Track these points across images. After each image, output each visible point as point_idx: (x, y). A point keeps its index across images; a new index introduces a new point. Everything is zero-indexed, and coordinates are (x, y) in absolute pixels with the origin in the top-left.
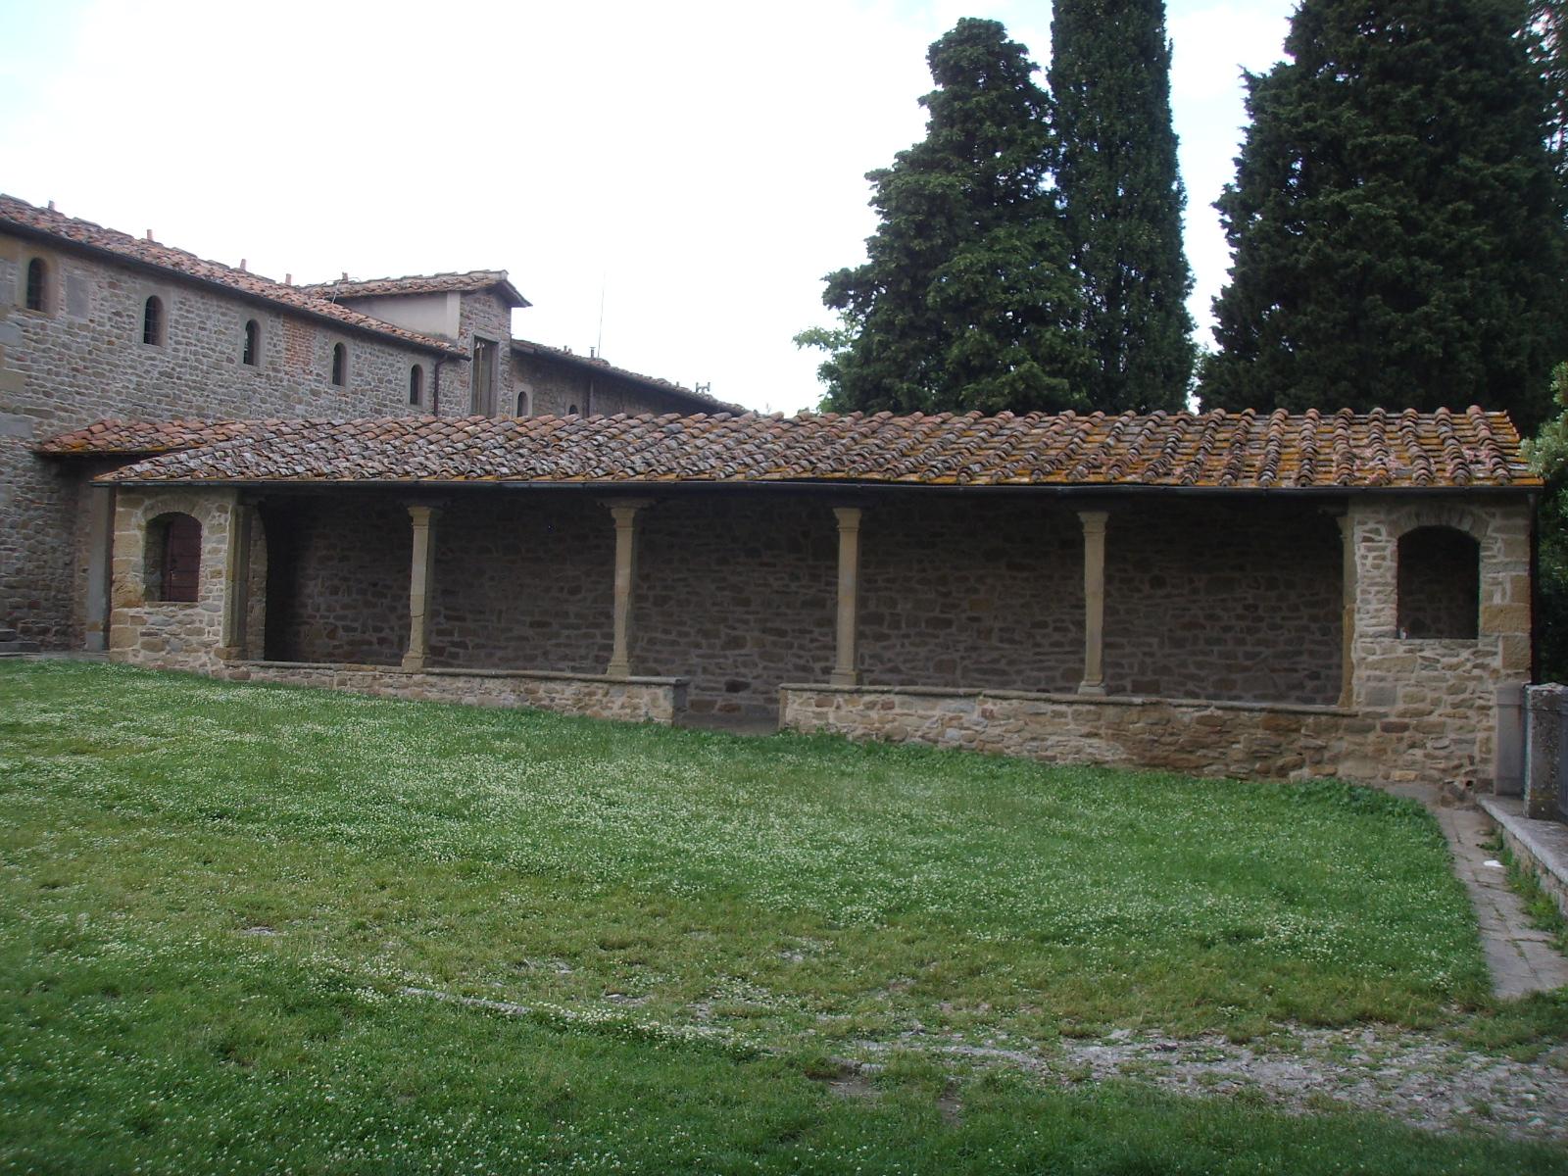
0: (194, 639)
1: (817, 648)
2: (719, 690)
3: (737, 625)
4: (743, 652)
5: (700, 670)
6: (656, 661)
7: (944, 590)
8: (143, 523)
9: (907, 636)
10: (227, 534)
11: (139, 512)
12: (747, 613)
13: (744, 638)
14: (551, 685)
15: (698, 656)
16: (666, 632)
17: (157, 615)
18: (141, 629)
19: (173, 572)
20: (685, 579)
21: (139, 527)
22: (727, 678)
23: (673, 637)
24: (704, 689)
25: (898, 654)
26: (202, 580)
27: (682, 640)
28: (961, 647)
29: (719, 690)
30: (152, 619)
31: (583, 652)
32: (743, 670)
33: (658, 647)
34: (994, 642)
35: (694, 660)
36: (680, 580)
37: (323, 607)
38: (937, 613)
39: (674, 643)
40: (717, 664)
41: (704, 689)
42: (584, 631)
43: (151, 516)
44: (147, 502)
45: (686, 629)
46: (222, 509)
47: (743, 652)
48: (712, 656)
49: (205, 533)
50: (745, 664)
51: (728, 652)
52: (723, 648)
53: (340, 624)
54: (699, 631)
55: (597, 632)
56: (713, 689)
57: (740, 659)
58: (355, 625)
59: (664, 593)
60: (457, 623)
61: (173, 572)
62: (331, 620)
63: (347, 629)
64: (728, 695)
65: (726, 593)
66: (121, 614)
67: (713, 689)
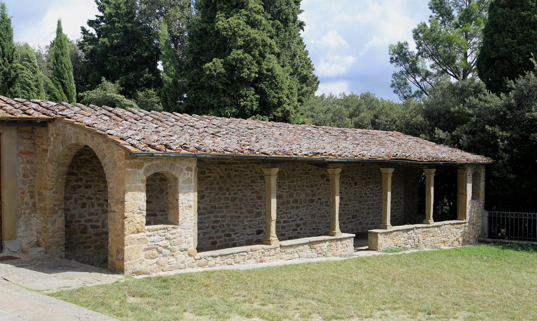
0: (176, 248)
1: (282, 214)
2: (254, 234)
3: (259, 207)
4: (261, 218)
5: (248, 227)
6: (234, 225)
7: (312, 189)
8: (145, 178)
9: (304, 207)
10: (193, 184)
11: (141, 171)
12: (261, 202)
13: (261, 212)
14: (321, 245)
15: (247, 221)
16: (236, 212)
17: (157, 233)
18: (145, 246)
19: (160, 211)
20: (241, 190)
21: (142, 181)
22: (257, 229)
23: (238, 214)
24: (249, 235)
25: (302, 213)
26: (180, 212)
27: (242, 215)
28: (317, 209)
29: (254, 234)
30: (152, 238)
31: (207, 225)
32: (261, 225)
33: (234, 219)
34: (324, 206)
35: (246, 223)
36: (239, 190)
37: (77, 216)
38: (311, 198)
39: (239, 217)
40: (253, 224)
41: (249, 235)
42: (207, 215)
43: (149, 174)
44: (146, 165)
45: (243, 211)
46: (189, 169)
47: (261, 218)
48: (251, 221)
49: (180, 183)
50: (262, 223)
51: (257, 219)
52: (255, 217)
53: (89, 224)
54: (247, 211)
55: (212, 215)
56: (252, 234)
57: (260, 221)
58: (98, 224)
59: (234, 196)
60: (152, 218)
61: (160, 211)
62: (83, 223)
63: (93, 227)
64: (257, 236)
65: (255, 194)
66: (131, 238)
67: (252, 234)
